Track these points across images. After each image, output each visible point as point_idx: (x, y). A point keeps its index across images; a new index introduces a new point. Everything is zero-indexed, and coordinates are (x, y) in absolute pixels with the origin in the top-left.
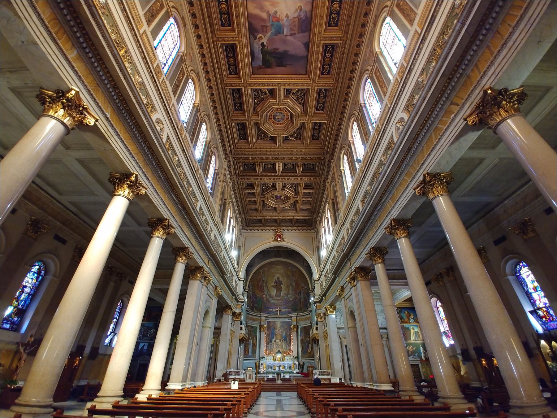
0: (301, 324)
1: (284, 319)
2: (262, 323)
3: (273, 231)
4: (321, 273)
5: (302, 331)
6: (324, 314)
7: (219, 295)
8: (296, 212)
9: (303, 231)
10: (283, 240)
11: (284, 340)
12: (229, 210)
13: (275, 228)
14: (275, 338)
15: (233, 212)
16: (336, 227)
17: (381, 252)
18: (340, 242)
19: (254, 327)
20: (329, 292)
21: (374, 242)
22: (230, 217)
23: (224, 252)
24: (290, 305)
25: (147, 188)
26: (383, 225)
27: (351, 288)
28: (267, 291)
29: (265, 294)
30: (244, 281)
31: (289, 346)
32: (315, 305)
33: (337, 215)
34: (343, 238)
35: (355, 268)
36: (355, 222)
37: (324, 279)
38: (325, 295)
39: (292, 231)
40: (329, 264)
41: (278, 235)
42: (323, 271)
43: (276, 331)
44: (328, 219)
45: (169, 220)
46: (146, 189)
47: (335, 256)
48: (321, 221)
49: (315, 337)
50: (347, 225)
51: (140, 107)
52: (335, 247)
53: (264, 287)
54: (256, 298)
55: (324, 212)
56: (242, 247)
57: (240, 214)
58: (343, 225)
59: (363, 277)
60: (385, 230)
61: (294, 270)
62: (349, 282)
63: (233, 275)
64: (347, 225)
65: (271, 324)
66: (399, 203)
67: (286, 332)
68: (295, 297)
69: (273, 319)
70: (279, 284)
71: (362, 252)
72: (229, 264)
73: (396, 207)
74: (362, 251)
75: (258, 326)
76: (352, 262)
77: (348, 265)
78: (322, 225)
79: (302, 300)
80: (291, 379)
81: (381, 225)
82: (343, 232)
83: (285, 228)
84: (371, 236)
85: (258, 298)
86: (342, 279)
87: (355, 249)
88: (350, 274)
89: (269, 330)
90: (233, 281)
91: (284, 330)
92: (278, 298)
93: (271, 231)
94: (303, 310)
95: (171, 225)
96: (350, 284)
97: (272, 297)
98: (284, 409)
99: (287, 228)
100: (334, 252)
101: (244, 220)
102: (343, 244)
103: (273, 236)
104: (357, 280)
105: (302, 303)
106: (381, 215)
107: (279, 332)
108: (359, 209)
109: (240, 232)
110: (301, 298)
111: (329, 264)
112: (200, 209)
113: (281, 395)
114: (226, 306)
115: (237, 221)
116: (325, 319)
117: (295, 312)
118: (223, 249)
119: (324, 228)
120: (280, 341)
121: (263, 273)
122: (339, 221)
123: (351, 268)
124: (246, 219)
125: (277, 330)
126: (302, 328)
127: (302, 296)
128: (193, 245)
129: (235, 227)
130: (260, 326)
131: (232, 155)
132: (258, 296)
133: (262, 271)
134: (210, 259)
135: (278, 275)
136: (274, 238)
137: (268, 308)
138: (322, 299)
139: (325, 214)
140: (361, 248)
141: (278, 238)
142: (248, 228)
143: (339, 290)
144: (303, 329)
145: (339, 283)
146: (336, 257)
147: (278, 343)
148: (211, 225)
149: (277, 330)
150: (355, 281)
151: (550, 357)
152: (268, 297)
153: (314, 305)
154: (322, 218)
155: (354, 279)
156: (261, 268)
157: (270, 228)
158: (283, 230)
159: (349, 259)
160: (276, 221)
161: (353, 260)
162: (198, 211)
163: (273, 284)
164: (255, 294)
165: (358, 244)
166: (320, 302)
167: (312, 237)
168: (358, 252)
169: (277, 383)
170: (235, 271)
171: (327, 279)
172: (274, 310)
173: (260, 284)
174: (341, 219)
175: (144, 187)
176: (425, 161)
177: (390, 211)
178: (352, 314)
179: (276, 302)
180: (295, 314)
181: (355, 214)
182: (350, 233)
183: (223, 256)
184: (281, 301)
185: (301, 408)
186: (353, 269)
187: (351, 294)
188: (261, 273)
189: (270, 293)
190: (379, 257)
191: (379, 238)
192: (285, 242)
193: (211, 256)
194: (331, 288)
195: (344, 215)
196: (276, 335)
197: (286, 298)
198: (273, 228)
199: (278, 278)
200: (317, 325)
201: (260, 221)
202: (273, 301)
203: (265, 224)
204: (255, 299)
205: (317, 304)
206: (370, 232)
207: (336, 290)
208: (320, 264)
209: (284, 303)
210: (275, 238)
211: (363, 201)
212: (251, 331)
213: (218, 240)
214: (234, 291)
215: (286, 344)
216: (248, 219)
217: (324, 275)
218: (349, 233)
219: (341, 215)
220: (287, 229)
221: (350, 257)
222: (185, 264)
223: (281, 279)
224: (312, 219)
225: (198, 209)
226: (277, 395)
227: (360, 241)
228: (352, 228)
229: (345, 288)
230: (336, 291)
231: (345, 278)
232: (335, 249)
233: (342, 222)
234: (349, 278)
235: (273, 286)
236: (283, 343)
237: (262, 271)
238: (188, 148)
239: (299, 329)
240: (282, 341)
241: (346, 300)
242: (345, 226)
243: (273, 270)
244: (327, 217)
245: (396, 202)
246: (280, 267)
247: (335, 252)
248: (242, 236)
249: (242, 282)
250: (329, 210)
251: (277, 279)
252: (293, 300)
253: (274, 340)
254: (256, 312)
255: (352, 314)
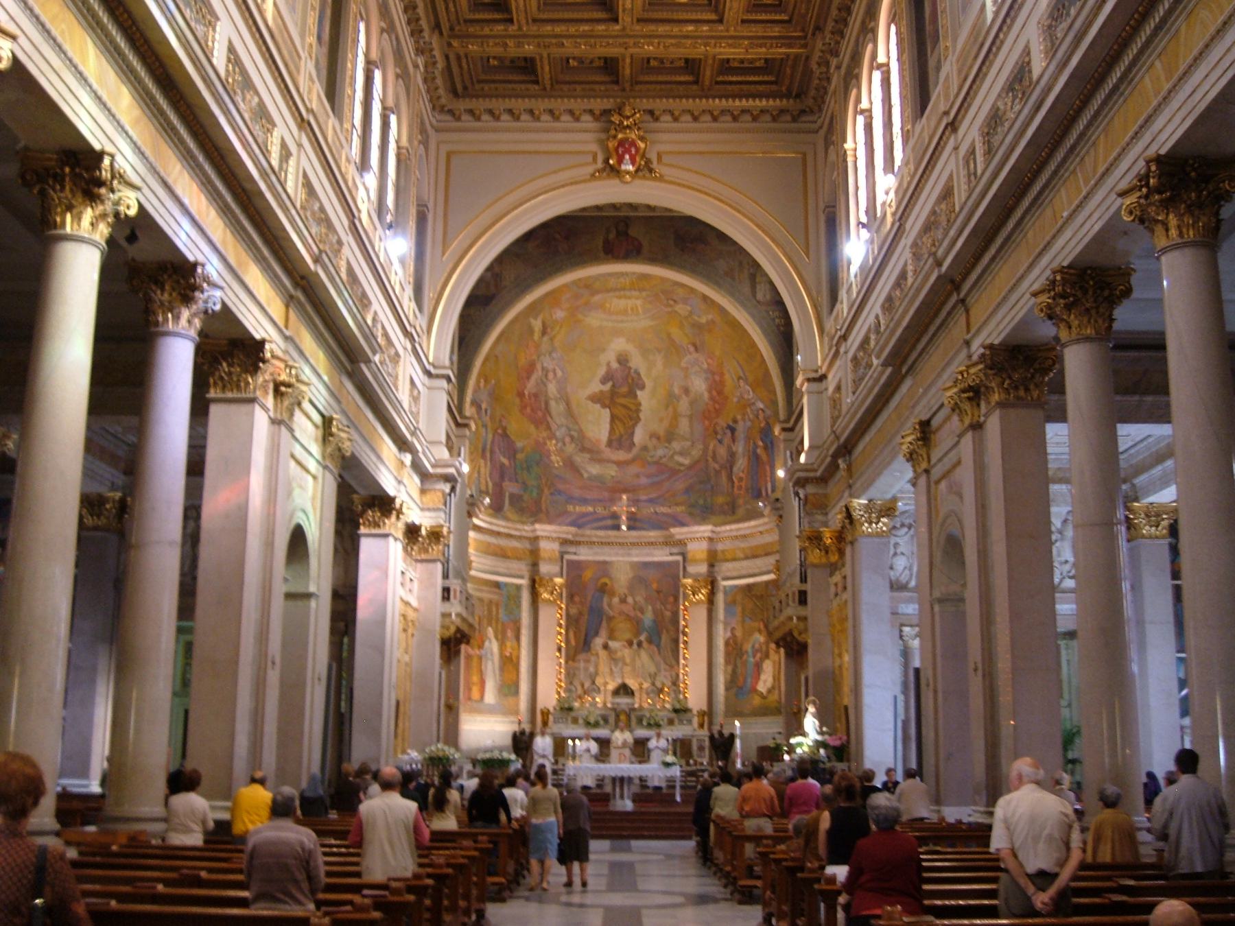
0: (729, 574)
1: (646, 550)
2: (544, 568)
3: (597, 119)
4: (838, 345)
5: (734, 602)
6: (840, 537)
7: (343, 457)
8: (721, 21)
9: (755, 119)
10: (651, 170)
11: (650, 641)
12: (362, 26)
13: (608, 104)
14: (603, 633)
15: (382, 30)
16: (918, 128)
17: (1102, 289)
18: (933, 212)
19: (506, 584)
20: (867, 438)
21: (1073, 243)
22: (385, 108)
23: (351, 252)
24: (680, 485)
25: (224, 285)
26: (1118, 173)
27: (960, 436)
28: (563, 421)
29: (552, 436)
30: (449, 379)
31: (671, 667)
32: (802, 493)
33: (932, 63)
34: (947, 194)
35: (982, 350)
36: (1007, 125)
37: (850, 376)
38: (846, 449)
39: (695, 119)
40: (875, 306)
41: (621, 143)
42: (844, 338)
43: (610, 605)
44: (871, 117)
45: (112, 156)
46: (13, 38)
47: (903, 275)
48: (852, 77)
49: (790, 633)
50: (971, 131)
51: (332, 283)
52: (908, 226)
53: (553, 404)
54: (512, 452)
55: (868, 30)
56: (431, 205)
57: (416, 33)
58: (953, 126)
59: (1016, 388)
60: (1119, 200)
61: (703, 320)
62: (955, 408)
63: (397, 354)
64: (971, 131)
65: (588, 574)
66: (1187, 88)
67: (658, 606)
68: (705, 450)
69: (596, 549)
70: (624, 390)
71: (1022, 278)
72: (375, 306)
73: (1175, 104)
74: (1021, 271)
75: (524, 582)
76: (977, 314)
77: (957, 329)
78: (858, 101)
79: (741, 464)
80: (674, 795)
81: (1108, 170)
82: (949, 166)
83: (659, 104)
84: (1065, 214)
85: (520, 456)
86: (930, 387)
87: (993, 259)
88: (961, 373)
89: (577, 599)
90: (400, 383)
91: (648, 599)
92: (621, 455)
93: (587, 122)
94: (741, 512)
95: (121, 176)
96: (955, 418)
97: (590, 451)
98: (640, 887)
99: (671, 103)
100: (903, 255)
101: (441, 65)
102: (943, 219)
103: (594, 147)
104: (988, 403)
105: (741, 479)
106: (1116, 118)
107: (625, 608)
108: (1029, 63)
109: (420, 131)
110: (732, 455)
111: (875, 306)
112: (229, 60)
113: (629, 850)
114: (374, 498)
115: (403, 76)
116: (841, 553)
117: (703, 520)
118: (347, 239)
119: (868, 114)
120: (630, 643)
121: (544, 333)
122: (939, 100)
123: (968, 343)
124: (452, 57)
125: (616, 600)
126: (735, 596)
127: (740, 448)
128: (219, 245)
129: (396, 110)
130: (533, 583)
131: (441, 34)
132: (519, 445)
133: (537, 324)
134: (291, 297)
135: (619, 345)
136: (600, 158)
137: (571, 499)
138: (833, 468)
139: (875, 42)
140: (1019, 257)
141: (620, 160)
142: (462, 105)
143: (909, 439)
144: (739, 598)
145: (914, 407)
146: (910, 280)
147: (619, 654)
148: (284, 129)
149: (616, 600)
150: (978, 405)
151: (592, 756)
152: (570, 448)
153: (797, 494)
154: (856, 59)
155: (975, 393)
156: (533, 309)
157: (577, 105)
158: (648, 117)
159: (963, 301)
160: (610, 66)
161: (980, 307)
162: (223, 74)
163: (596, 387)
164: (505, 435)
165: (920, 354)
166: (824, 480)
167: (804, 155)
168: (1003, 276)
169: (611, 808)
170: (407, 334)
171: (862, 379)
172: (600, 510)
173: (531, 386)
174: (947, 96)
175: (215, 286)
176: (1191, 66)
177: (1150, 117)
178: (953, 547)
179: (612, 471)
180: (705, 530)
181: (1010, 88)
182: (979, 172)
183: (350, 271)
184: (634, 469)
185: (705, 885)
186: (977, 348)
187: (959, 463)
188: (536, 336)
189: (581, 431)
190: (1087, 310)
191: (1097, 228)
192: (661, 179)
193: (296, 285)
194: (879, 423)
195: (960, 71)
196: (610, 619)
197: (660, 452)
198: (599, 104)
199: (623, 360)
200: (804, 579)
201: (527, 67)
202: (594, 469)
203: (555, 82)
204: (505, 461)
205: (811, 489)
206: (1063, 192)
207: (898, 432)
208: (834, 298)
209: (648, 476)
210: (606, 161)
211: (1049, 30)
212: (491, 602)
213: (257, 93)
214: (407, 427)
215: (658, 658)
216: (458, 58)
217: (850, 355)
218: (975, 174)
219: (948, 76)
220: (671, 113)
221: (967, 294)
222: (192, 339)
223: (637, 362)
224: (807, 58)
225: (220, 58)
226: (613, 850)
227: (1019, 223)
228: (990, 152)
229: (938, 429)
230: (898, 439)
231: (940, 384)
232: (906, 241)
233: (946, 113)
234: (955, 390)
235: (596, 399)
236: (643, 654)
237: (537, 324)
238: (292, 57)
239: (720, 599)
240: (640, 644)
241: (938, 482)
242: (961, 131)
243: (594, 320)
244: (881, 59)
245: (1180, 79)
246: (630, 303)
247: (907, 255)
248: (432, 146)
249: (444, 383)
250: (893, 28)
251: (615, 365)
252: (690, 467)
253: (598, 642)
254: (509, 515)
255: (953, 547)
